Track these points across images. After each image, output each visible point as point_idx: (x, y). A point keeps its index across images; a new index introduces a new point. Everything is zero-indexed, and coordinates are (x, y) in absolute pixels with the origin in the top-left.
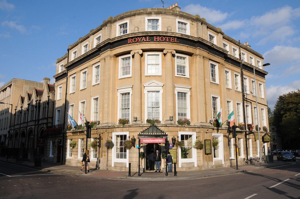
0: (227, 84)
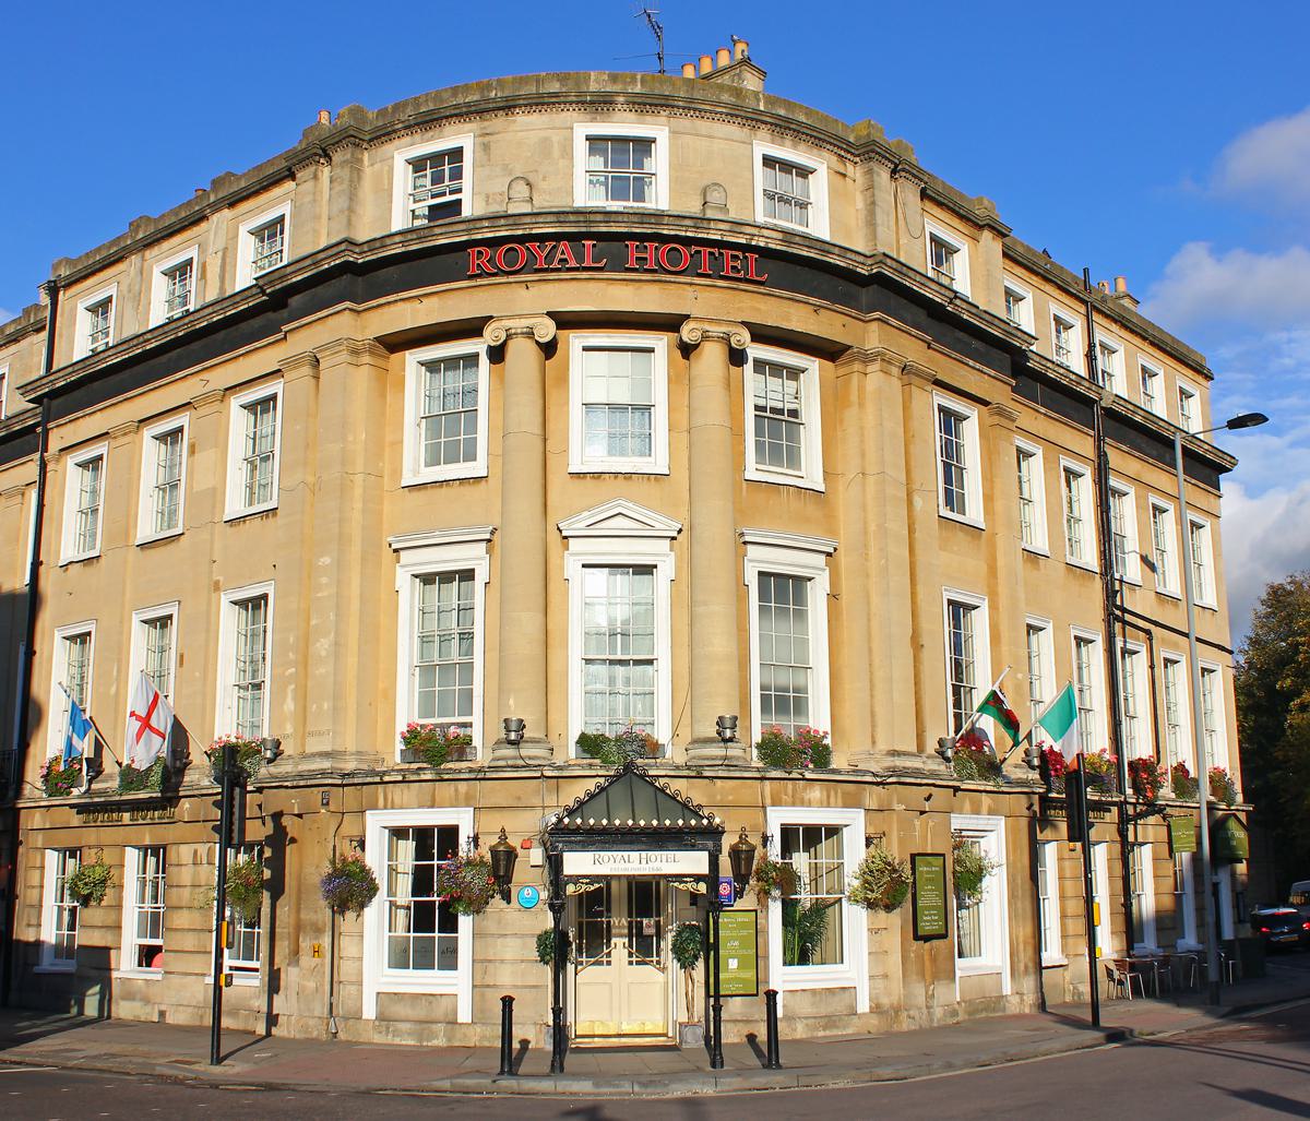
0: (1021, 527)
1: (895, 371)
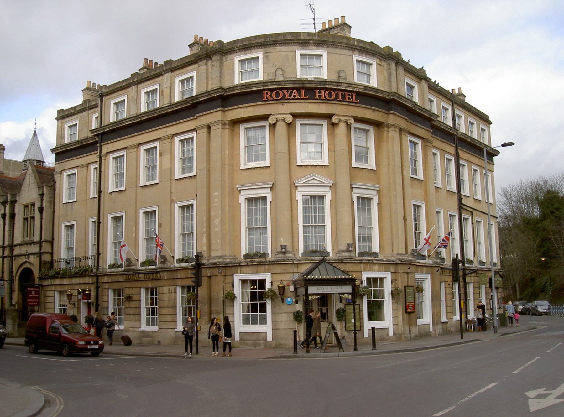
1: (398, 130)
